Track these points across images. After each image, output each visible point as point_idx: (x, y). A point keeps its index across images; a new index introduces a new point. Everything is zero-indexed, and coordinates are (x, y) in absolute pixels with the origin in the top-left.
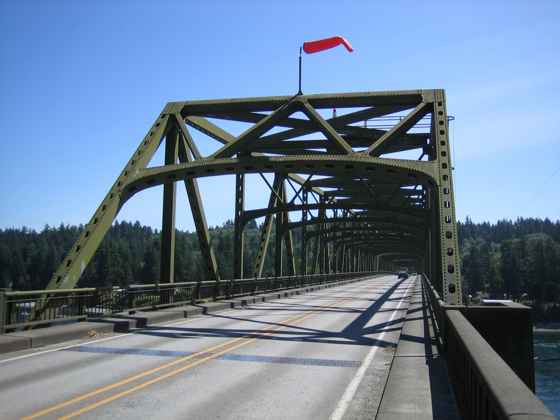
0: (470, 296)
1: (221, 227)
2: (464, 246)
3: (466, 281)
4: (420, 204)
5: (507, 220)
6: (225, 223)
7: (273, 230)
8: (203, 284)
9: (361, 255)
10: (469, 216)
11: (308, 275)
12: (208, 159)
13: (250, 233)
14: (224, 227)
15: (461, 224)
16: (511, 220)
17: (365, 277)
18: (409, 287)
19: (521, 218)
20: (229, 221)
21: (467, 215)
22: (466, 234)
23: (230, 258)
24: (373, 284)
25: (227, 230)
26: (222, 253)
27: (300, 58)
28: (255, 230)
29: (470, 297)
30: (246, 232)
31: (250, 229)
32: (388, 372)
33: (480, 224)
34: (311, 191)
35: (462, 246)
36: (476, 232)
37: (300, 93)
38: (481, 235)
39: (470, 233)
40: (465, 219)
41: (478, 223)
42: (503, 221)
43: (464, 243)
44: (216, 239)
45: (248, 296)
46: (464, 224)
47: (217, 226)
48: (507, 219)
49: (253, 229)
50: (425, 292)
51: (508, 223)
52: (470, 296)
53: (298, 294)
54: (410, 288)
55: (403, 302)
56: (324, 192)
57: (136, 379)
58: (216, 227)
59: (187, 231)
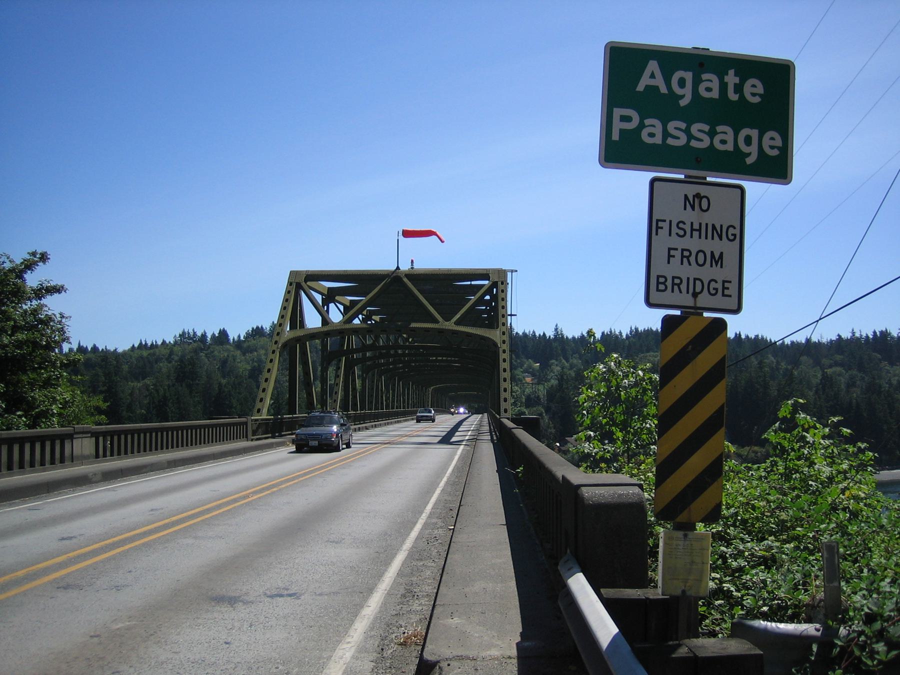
0: (558, 444)
1: (170, 342)
2: (552, 371)
3: (551, 423)
4: (486, 308)
5: (615, 332)
6: (178, 336)
7: (257, 347)
8: (286, 418)
9: (412, 388)
10: (558, 326)
11: (299, 414)
12: (339, 324)
13: (220, 352)
14: (176, 342)
15: (548, 338)
16: (620, 331)
17: (375, 422)
18: (472, 429)
19: (635, 328)
20: (184, 333)
21: (555, 324)
22: (555, 353)
23: (196, 393)
24: (419, 426)
25: (181, 347)
26: (184, 385)
27: (398, 240)
28: (228, 346)
29: (557, 445)
30: (212, 350)
31: (220, 346)
32: (469, 478)
33: (575, 338)
34: (334, 301)
35: (549, 370)
36: (569, 350)
37: (398, 268)
38: (577, 354)
39: (560, 352)
40: (554, 330)
41: (572, 336)
42: (609, 333)
43: (550, 367)
44: (164, 361)
45: (270, 439)
46: (552, 337)
47: (163, 340)
48: (614, 330)
49: (224, 346)
50: (493, 433)
51: (617, 337)
52: (558, 444)
53: (368, 429)
54: (472, 430)
55: (466, 445)
56: (349, 302)
57: (208, 514)
58: (162, 341)
59: (116, 350)
